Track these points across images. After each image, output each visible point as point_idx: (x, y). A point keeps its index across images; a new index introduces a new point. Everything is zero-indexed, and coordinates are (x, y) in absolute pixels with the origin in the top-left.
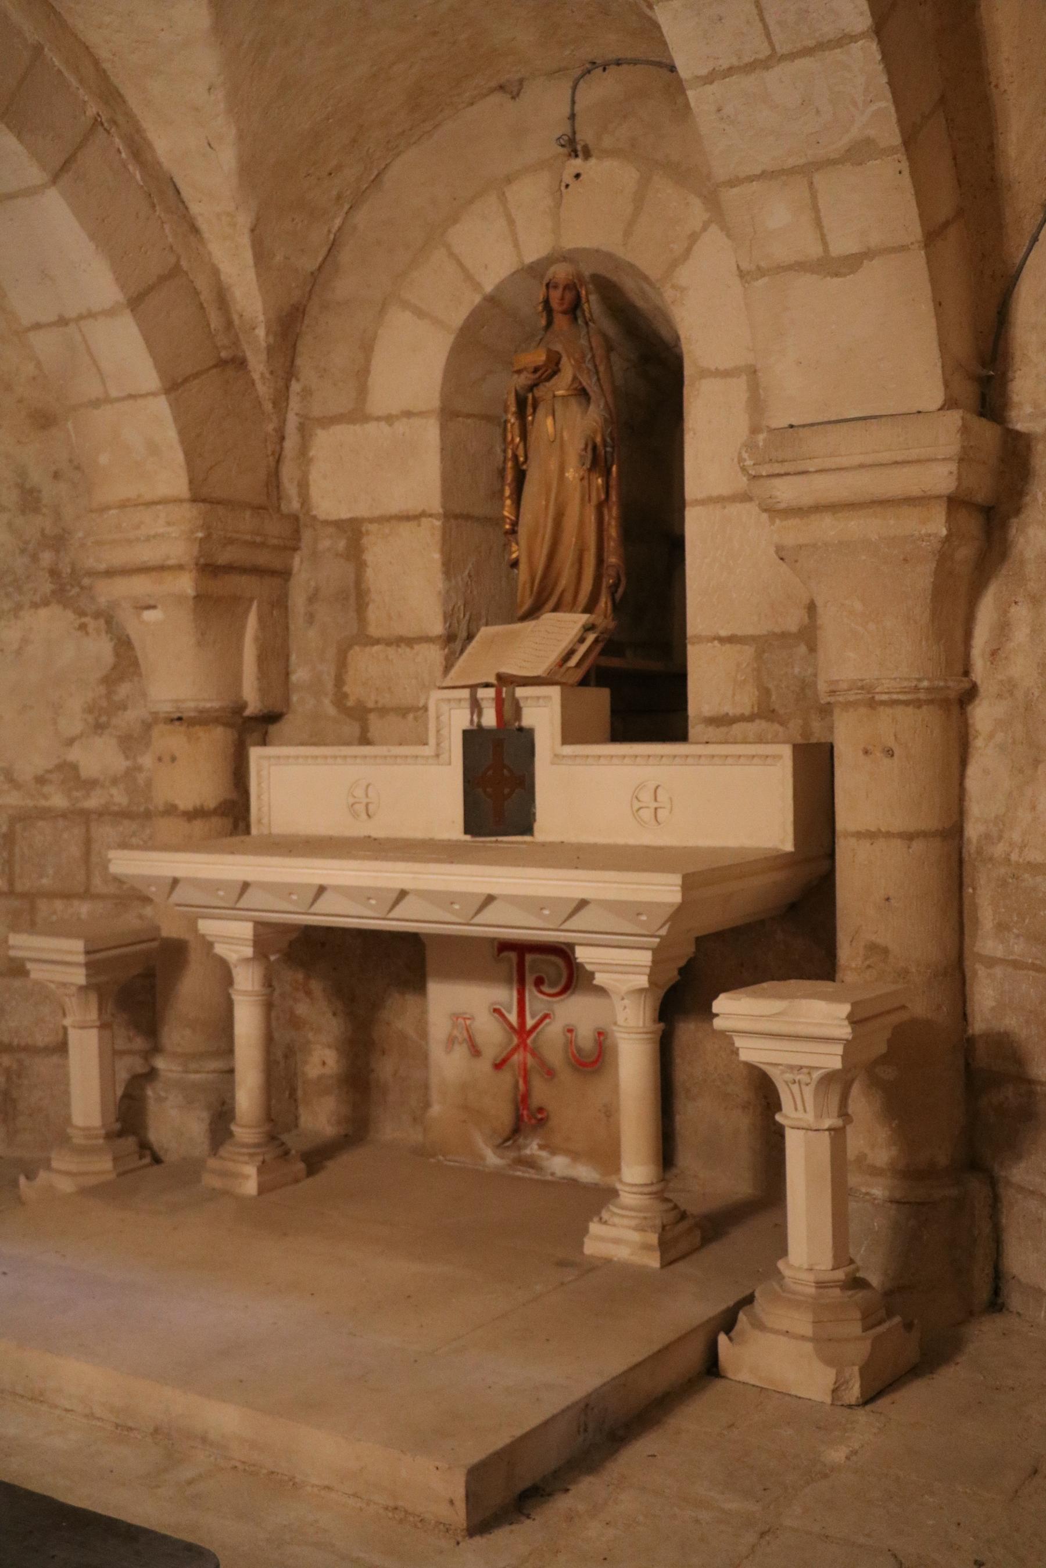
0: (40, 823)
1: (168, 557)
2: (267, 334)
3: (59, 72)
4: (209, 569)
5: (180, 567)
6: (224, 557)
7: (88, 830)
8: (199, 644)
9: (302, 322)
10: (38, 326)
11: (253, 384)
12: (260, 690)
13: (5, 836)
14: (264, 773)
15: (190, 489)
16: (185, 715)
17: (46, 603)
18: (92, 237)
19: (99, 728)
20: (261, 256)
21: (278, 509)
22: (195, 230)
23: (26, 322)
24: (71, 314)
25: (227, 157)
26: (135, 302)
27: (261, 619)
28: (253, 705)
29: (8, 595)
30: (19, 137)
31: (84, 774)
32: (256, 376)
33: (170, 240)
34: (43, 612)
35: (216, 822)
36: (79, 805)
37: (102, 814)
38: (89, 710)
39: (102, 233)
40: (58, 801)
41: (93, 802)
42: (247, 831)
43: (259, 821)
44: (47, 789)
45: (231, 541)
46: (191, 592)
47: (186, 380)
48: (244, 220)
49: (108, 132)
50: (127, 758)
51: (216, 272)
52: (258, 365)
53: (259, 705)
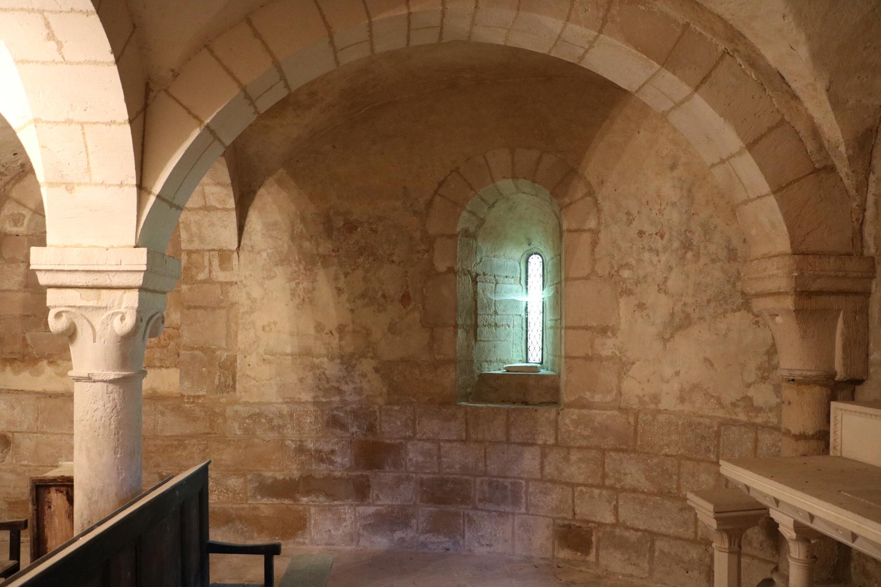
0: (733, 428)
1: (780, 288)
2: (847, 150)
3: (700, 33)
4: (803, 294)
5: (787, 293)
6: (815, 286)
7: (756, 434)
8: (803, 337)
9: (876, 138)
10: (713, 166)
11: (841, 180)
12: (844, 365)
13: (716, 432)
14: (839, 418)
15: (792, 247)
16: (796, 378)
17: (739, 310)
18: (722, 115)
19: (764, 379)
20: (836, 103)
21: (862, 254)
22: (795, 97)
23: (709, 164)
24: (724, 157)
25: (803, 52)
26: (751, 146)
27: (845, 322)
28: (840, 375)
29: (721, 305)
30: (674, 73)
31: (755, 404)
32: (842, 175)
33: (776, 106)
34: (737, 314)
35: (813, 444)
36: (752, 420)
37: (764, 426)
38: (759, 369)
39: (728, 113)
40: (742, 417)
41: (759, 420)
42: (828, 453)
43: (835, 448)
44: (738, 410)
45: (819, 277)
46: (792, 308)
47: (788, 184)
48: (821, 85)
49: (733, 56)
50: (778, 397)
51: (811, 118)
52: (843, 169)
53: (844, 375)
